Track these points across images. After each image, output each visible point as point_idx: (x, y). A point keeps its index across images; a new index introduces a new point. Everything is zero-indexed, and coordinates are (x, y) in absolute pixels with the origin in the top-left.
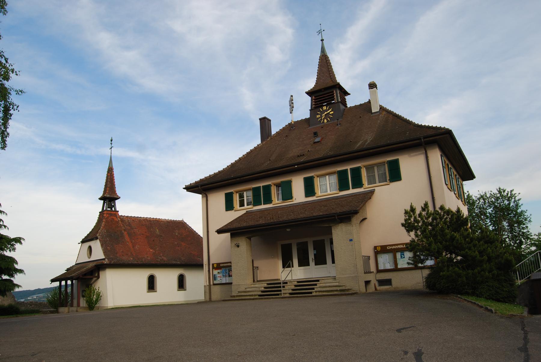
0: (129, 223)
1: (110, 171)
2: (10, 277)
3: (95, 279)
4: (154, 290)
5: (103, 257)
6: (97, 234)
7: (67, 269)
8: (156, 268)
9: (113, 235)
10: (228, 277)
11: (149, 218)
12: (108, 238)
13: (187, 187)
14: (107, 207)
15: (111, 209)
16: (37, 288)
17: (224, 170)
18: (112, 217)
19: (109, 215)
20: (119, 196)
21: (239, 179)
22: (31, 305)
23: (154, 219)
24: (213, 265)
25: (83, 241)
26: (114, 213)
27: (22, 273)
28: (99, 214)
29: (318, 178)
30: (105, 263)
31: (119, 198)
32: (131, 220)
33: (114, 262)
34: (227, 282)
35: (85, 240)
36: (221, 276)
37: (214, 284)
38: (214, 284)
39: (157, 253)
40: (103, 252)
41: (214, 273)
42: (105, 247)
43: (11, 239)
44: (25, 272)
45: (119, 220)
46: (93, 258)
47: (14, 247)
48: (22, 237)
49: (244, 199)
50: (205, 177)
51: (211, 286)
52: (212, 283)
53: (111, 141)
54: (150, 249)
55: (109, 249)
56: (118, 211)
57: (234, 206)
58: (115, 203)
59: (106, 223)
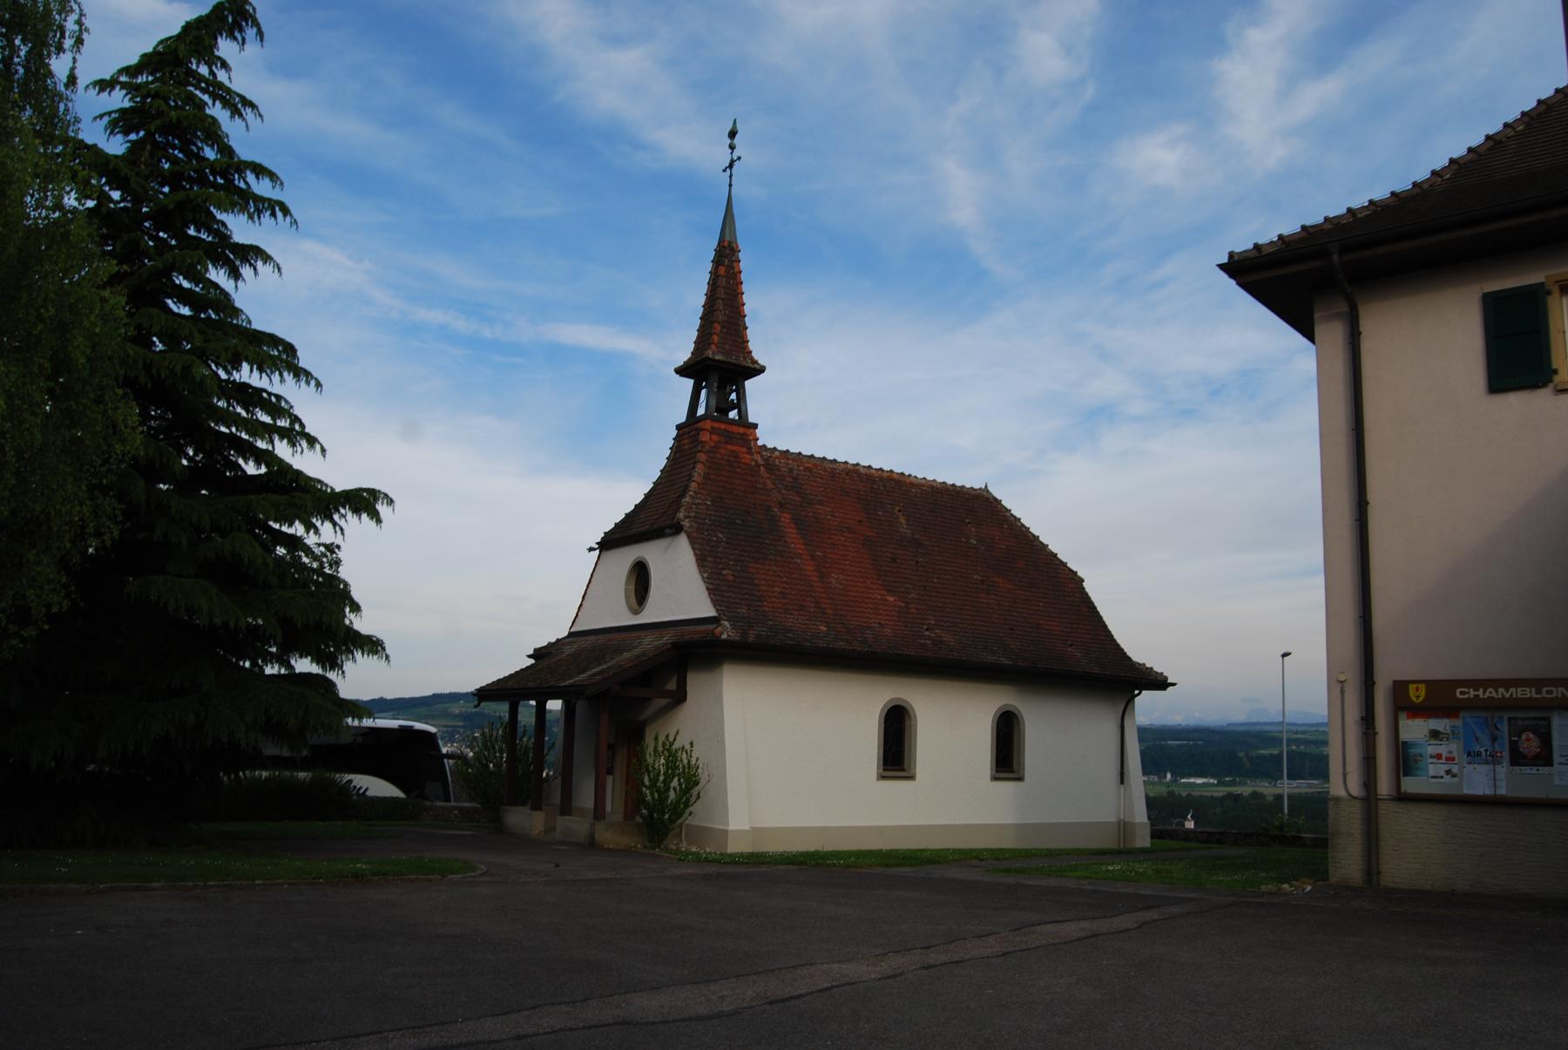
0: (795, 479)
2: (324, 668)
3: (661, 702)
4: (903, 770)
5: (706, 610)
6: (677, 510)
7: (535, 650)
8: (888, 679)
9: (739, 522)
10: (1506, 762)
11: (864, 467)
12: (722, 533)
14: (713, 403)
16: (377, 697)
18: (729, 447)
19: (723, 439)
20: (761, 362)
23: (885, 474)
24: (1400, 688)
25: (608, 543)
26: (741, 430)
27: (377, 652)
30: (724, 636)
31: (761, 370)
32: (801, 468)
34: (1502, 791)
35: (618, 536)
36: (1455, 754)
37: (1402, 798)
38: (1402, 798)
39: (913, 611)
40: (707, 589)
41: (1404, 736)
42: (715, 570)
43: (337, 493)
44: (388, 651)
46: (654, 613)
47: (334, 555)
51: (1382, 805)
52: (1384, 787)
53: (733, 134)
54: (886, 593)
55: (731, 578)
56: (755, 426)
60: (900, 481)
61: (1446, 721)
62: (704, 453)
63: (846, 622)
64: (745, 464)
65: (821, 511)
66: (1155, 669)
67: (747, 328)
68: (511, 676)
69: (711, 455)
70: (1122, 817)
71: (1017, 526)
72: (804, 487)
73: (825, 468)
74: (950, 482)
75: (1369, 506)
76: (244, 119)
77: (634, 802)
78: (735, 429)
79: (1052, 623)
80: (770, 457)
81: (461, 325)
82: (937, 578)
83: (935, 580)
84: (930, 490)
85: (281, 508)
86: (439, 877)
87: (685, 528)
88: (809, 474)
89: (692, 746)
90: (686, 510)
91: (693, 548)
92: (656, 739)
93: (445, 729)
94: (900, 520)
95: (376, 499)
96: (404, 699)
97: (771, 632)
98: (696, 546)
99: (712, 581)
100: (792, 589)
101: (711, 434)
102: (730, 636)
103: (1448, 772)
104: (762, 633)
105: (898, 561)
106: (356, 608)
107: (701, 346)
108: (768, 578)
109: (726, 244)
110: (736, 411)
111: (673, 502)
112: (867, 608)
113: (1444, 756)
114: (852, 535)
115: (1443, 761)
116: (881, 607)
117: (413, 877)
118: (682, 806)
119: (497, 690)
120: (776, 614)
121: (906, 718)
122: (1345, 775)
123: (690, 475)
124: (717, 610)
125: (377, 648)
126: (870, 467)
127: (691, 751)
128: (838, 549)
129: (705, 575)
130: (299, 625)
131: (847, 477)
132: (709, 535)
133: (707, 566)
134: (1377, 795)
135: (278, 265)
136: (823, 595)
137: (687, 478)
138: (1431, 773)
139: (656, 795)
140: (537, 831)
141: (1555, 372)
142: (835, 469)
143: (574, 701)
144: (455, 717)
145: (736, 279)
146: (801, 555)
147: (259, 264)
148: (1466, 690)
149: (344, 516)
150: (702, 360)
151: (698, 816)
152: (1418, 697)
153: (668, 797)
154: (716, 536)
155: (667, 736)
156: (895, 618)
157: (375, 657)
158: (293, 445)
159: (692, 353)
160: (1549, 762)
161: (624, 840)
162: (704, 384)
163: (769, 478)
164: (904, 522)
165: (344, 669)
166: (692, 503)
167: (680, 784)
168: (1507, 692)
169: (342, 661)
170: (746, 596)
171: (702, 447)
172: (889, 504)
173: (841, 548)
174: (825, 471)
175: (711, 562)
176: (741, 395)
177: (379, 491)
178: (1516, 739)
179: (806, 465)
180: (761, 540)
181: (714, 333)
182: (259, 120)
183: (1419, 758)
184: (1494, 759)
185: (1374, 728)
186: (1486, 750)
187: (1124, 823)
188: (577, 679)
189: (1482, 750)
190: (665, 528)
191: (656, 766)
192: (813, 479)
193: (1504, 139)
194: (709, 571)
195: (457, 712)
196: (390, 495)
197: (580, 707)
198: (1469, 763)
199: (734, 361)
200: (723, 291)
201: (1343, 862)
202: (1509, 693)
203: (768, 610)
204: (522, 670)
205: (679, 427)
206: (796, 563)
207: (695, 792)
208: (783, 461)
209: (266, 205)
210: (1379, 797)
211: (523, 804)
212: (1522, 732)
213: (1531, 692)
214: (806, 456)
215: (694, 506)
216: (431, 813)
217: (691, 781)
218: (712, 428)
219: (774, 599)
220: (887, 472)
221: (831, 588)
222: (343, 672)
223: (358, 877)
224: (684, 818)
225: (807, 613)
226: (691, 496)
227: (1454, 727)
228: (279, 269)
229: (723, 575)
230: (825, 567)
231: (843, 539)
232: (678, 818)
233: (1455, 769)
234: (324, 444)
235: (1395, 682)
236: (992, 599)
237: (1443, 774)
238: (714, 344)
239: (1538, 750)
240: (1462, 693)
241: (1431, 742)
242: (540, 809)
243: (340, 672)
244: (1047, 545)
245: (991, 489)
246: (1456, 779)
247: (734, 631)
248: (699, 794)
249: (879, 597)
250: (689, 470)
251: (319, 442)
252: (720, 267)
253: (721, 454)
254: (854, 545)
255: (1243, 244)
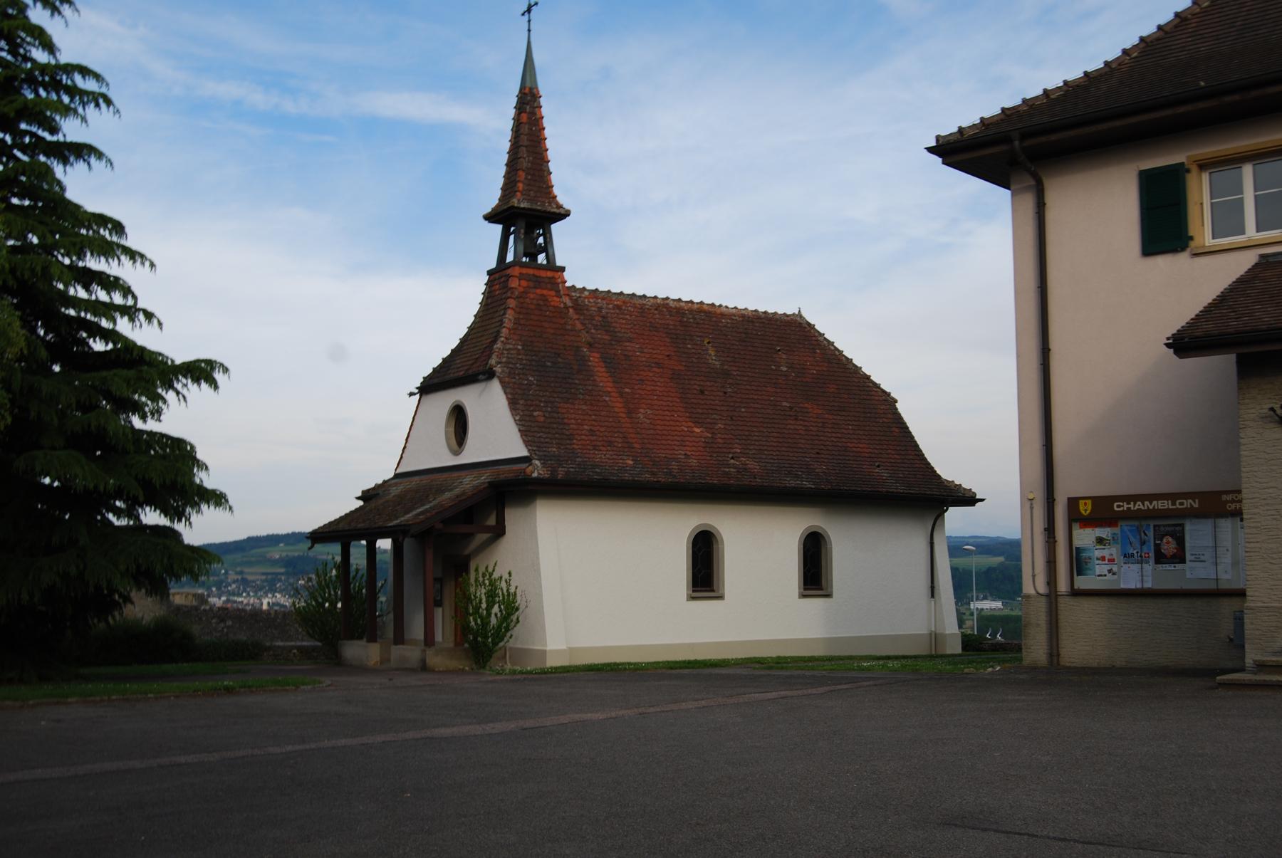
0: (603, 317)
1: (528, 103)
2: (172, 521)
3: (482, 537)
4: (713, 591)
6: (489, 357)
7: (363, 492)
9: (549, 364)
10: (1152, 561)
11: (674, 300)
12: (533, 376)
13: (948, 143)
14: (521, 249)
15: (533, 257)
17: (1112, 70)
18: (538, 291)
19: (531, 284)
20: (566, 206)
21: (1237, 97)
22: (223, 620)
23: (696, 306)
24: (1073, 503)
25: (429, 387)
26: (549, 274)
28: (486, 278)
29: (1205, 177)
30: (535, 475)
32: (611, 306)
33: (567, 473)
34: (1148, 585)
35: (436, 381)
36: (1115, 557)
37: (1076, 593)
38: (1076, 593)
40: (520, 430)
41: (1077, 542)
42: (526, 413)
44: (230, 503)
45: (569, 303)
46: (474, 452)
48: (219, 360)
49: (1242, 199)
50: (1025, 101)
51: (1061, 600)
52: (1063, 586)
54: (693, 425)
56: (562, 269)
57: (1191, 234)
58: (548, 236)
59: (519, 313)
60: (710, 312)
61: (1108, 529)
62: (514, 299)
63: (652, 455)
64: (554, 307)
65: (630, 348)
66: (963, 486)
67: (551, 173)
68: (341, 518)
69: (521, 300)
70: (933, 629)
71: (829, 349)
72: (614, 324)
73: (634, 304)
74: (761, 309)
75: (1051, 352)
76: (63, 16)
77: (462, 631)
78: (543, 274)
79: (861, 446)
80: (580, 297)
81: (259, 99)
82: (744, 407)
83: (743, 410)
84: (741, 319)
85: (132, 382)
86: (294, 688)
87: (498, 374)
88: (617, 311)
89: (510, 576)
90: (498, 356)
91: (505, 393)
92: (477, 570)
93: (264, 577)
94: (710, 352)
95: (213, 369)
96: (215, 544)
97: (579, 468)
98: (508, 390)
99: (523, 422)
100: (601, 426)
101: (519, 280)
102: (539, 474)
103: (1110, 571)
104: (572, 470)
105: (706, 393)
106: (203, 466)
107: (507, 192)
108: (577, 417)
109: (527, 91)
110: (544, 254)
111: (486, 348)
112: (673, 441)
113: (1107, 558)
114: (661, 370)
115: (1106, 562)
116: (687, 438)
117: (273, 688)
118: (503, 630)
119: (329, 532)
120: (585, 451)
121: (714, 542)
122: (1034, 576)
123: (502, 322)
124: (529, 450)
125: (221, 500)
126: (680, 300)
127: (510, 580)
128: (646, 384)
129: (517, 418)
130: (158, 487)
131: (656, 312)
132: (520, 378)
133: (518, 409)
134: (1056, 592)
135: (110, 160)
136: (631, 431)
137: (497, 324)
138: (1098, 573)
139: (479, 621)
140: (373, 663)
141: (1191, 238)
142: (645, 305)
143: (400, 539)
144: (274, 562)
145: (539, 126)
146: (609, 392)
147: (93, 160)
148: (1121, 504)
149: (185, 385)
150: (509, 208)
151: (519, 638)
152: (1086, 510)
153: (490, 622)
154: (528, 379)
155: (487, 568)
156: (702, 449)
157: (221, 508)
158: (132, 320)
159: (499, 199)
160: (1183, 561)
161: (453, 664)
162: (512, 229)
163: (578, 319)
164: (713, 353)
165: (191, 520)
166: (503, 349)
167: (501, 611)
168: (1151, 504)
169: (190, 514)
170: (557, 436)
171: (512, 293)
172: (698, 336)
173: (649, 383)
174: (636, 307)
175: (522, 404)
176: (548, 240)
177: (215, 361)
178: (1159, 542)
179: (616, 303)
180: (570, 381)
181: (519, 181)
182: (76, 14)
183: (1089, 561)
184: (1142, 561)
185: (1054, 538)
186: (1137, 552)
187: (936, 634)
188: (402, 519)
189: (1135, 552)
190: (479, 374)
191: (478, 595)
192: (621, 316)
193: (1189, 16)
194: (521, 414)
195: (277, 557)
196: (226, 364)
197: (408, 544)
198: (1125, 563)
199: (539, 208)
200: (526, 137)
201: (1032, 648)
202: (1153, 505)
203: (577, 447)
204: (352, 512)
205: (490, 273)
206: (605, 401)
207: (514, 618)
208: (591, 300)
209: (91, 97)
210: (1059, 593)
211: (360, 638)
212: (1163, 536)
213: (1168, 504)
214: (615, 293)
215: (505, 352)
216: (271, 652)
217: (511, 608)
218: (520, 274)
219: (583, 437)
220: (697, 303)
221: (638, 423)
222: (190, 523)
223: (229, 690)
224: (506, 639)
225: (615, 449)
226: (502, 342)
227: (1114, 534)
228: (111, 164)
229: (534, 417)
230: (633, 403)
231: (651, 374)
232: (500, 642)
233: (1115, 569)
234: (160, 319)
235: (1069, 499)
236: (801, 425)
237: (1107, 573)
238: (519, 191)
239: (1175, 551)
240: (1118, 506)
241: (1097, 547)
242: (375, 641)
243: (187, 523)
244: (861, 368)
245: (804, 314)
246: (1116, 577)
247: (545, 469)
248: (518, 619)
249: (686, 429)
250: (500, 316)
251: (155, 317)
252: (523, 114)
253: (530, 299)
254: (662, 380)
255: (949, 128)
